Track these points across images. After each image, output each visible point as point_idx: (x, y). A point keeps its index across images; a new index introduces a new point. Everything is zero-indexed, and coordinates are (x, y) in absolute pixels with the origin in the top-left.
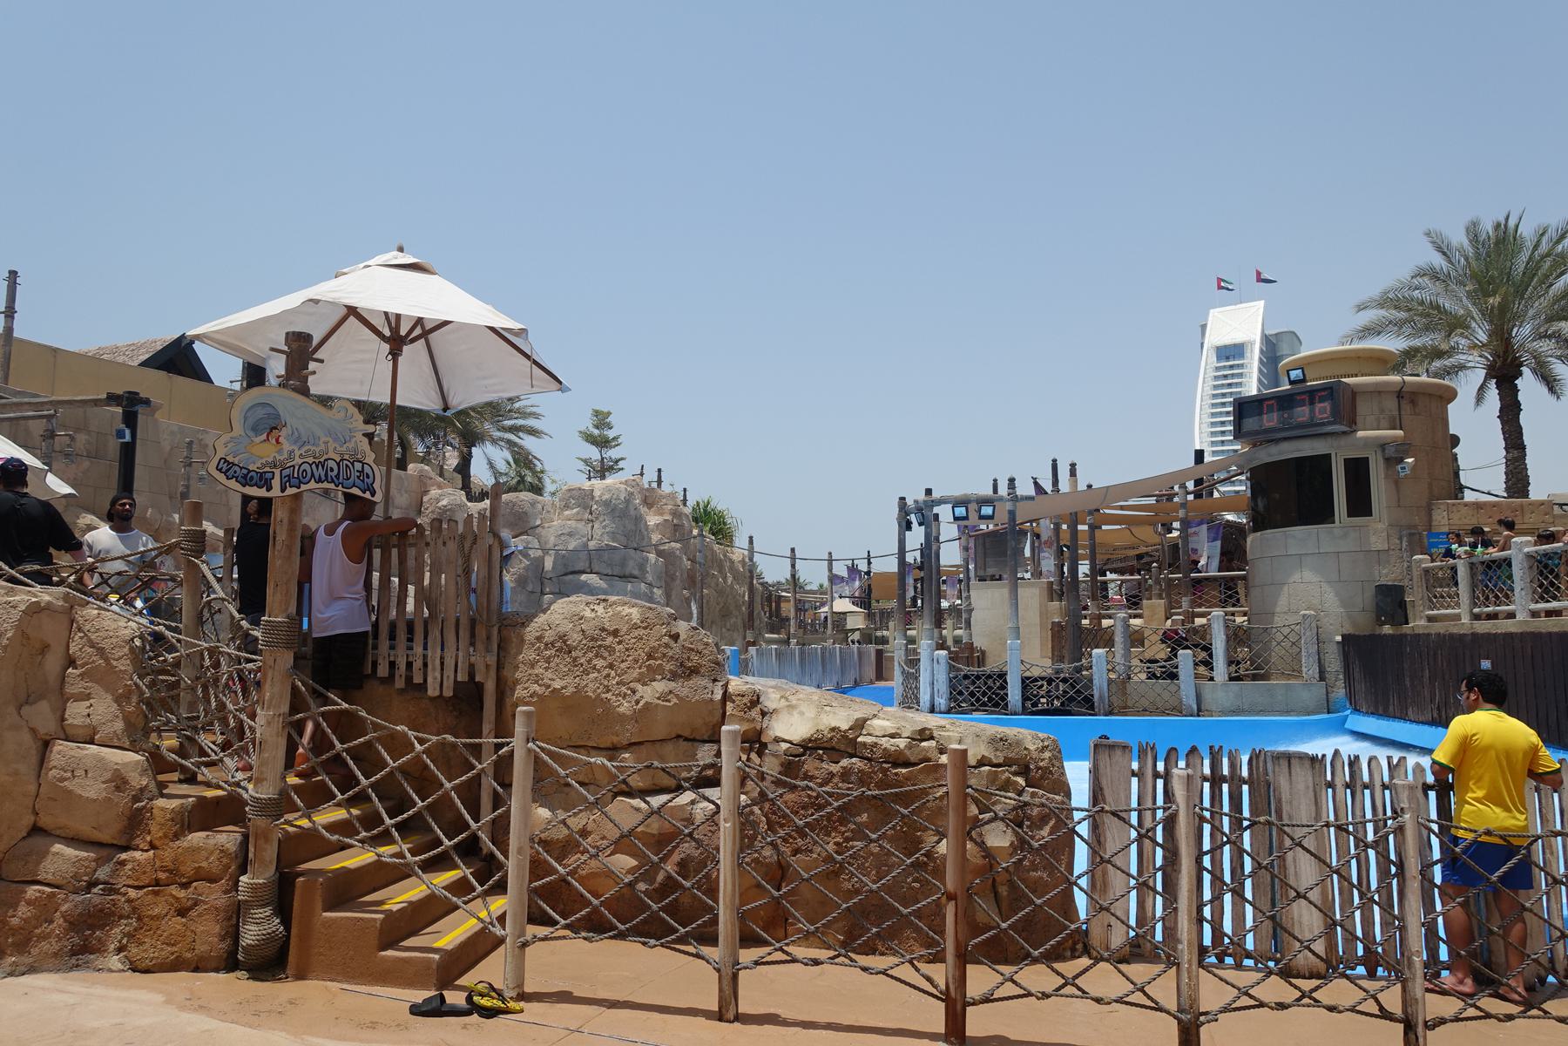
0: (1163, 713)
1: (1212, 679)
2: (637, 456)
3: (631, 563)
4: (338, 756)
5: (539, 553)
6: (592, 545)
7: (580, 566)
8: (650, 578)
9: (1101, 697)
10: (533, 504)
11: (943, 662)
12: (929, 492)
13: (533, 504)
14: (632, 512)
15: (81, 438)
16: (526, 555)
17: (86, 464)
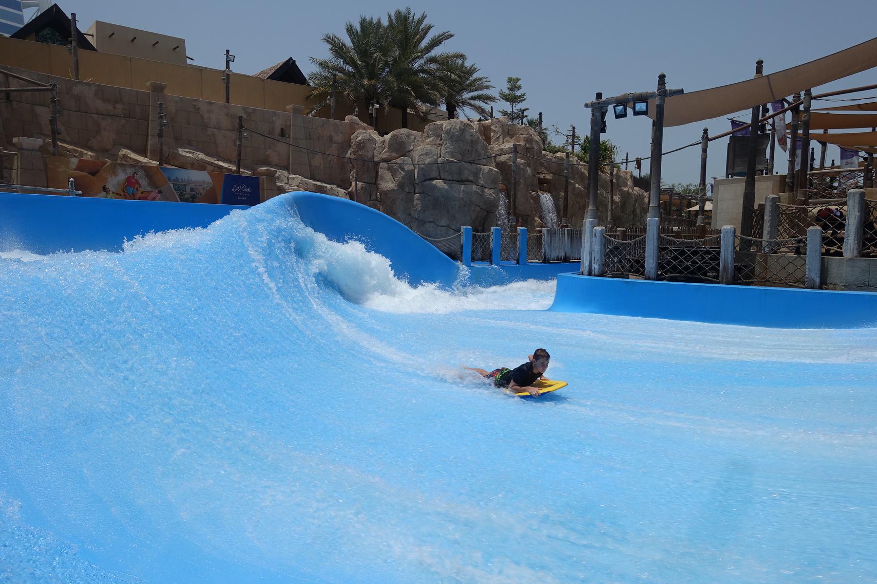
0: (786, 285)
1: (840, 254)
2: (532, 109)
3: (466, 172)
4: (700, 266)
5: (411, 167)
6: (439, 160)
7: (433, 176)
8: (482, 182)
9: (725, 268)
10: (408, 136)
11: (598, 235)
12: (599, 96)
13: (408, 136)
14: (468, 137)
15: (119, 107)
16: (403, 169)
17: (123, 121)
